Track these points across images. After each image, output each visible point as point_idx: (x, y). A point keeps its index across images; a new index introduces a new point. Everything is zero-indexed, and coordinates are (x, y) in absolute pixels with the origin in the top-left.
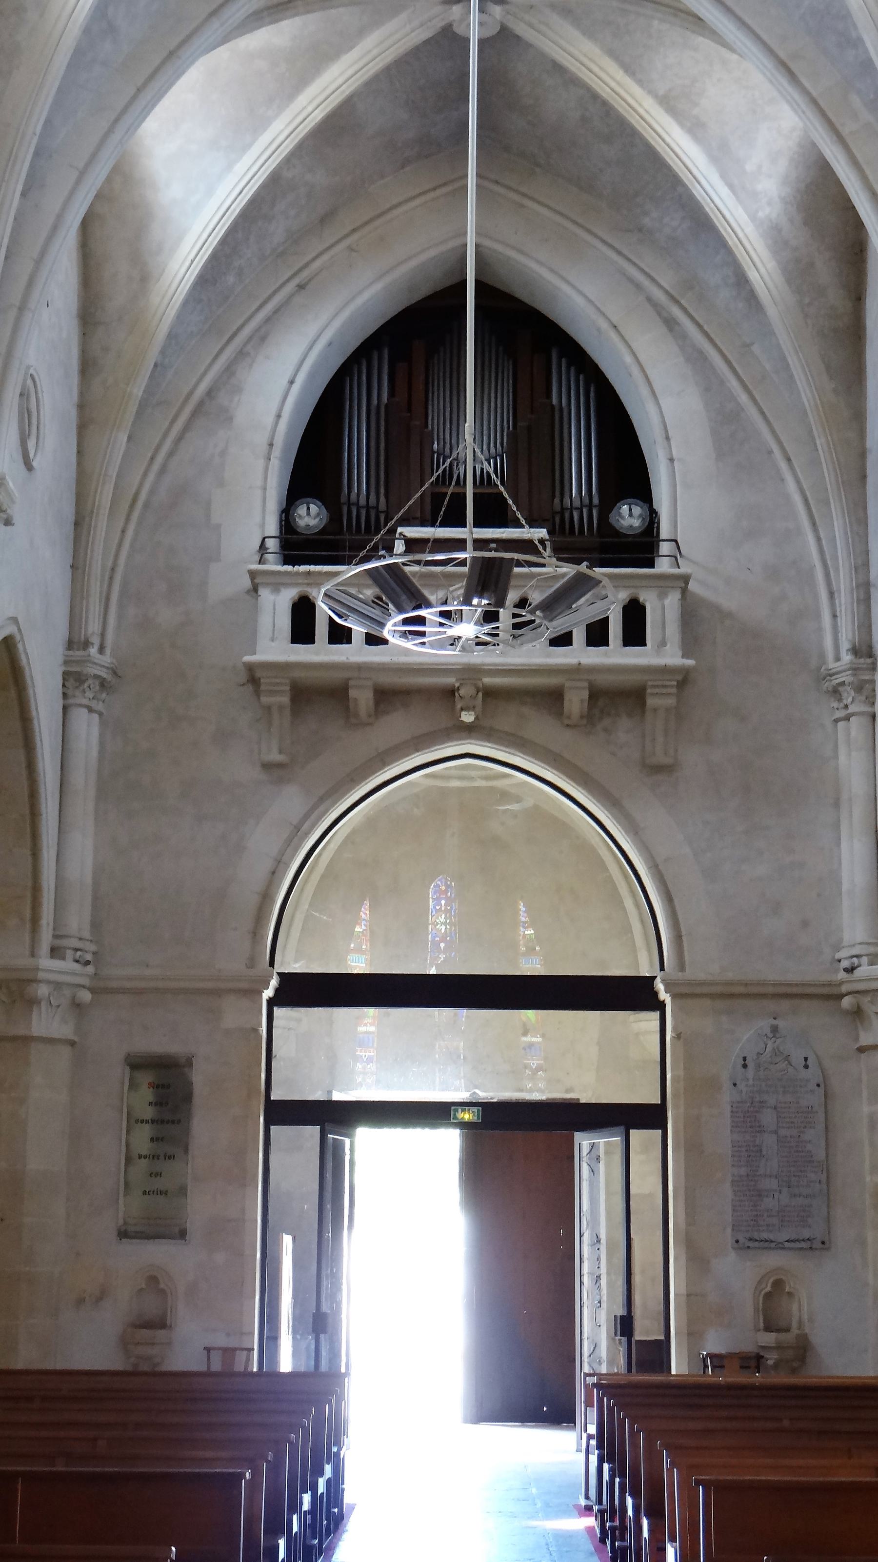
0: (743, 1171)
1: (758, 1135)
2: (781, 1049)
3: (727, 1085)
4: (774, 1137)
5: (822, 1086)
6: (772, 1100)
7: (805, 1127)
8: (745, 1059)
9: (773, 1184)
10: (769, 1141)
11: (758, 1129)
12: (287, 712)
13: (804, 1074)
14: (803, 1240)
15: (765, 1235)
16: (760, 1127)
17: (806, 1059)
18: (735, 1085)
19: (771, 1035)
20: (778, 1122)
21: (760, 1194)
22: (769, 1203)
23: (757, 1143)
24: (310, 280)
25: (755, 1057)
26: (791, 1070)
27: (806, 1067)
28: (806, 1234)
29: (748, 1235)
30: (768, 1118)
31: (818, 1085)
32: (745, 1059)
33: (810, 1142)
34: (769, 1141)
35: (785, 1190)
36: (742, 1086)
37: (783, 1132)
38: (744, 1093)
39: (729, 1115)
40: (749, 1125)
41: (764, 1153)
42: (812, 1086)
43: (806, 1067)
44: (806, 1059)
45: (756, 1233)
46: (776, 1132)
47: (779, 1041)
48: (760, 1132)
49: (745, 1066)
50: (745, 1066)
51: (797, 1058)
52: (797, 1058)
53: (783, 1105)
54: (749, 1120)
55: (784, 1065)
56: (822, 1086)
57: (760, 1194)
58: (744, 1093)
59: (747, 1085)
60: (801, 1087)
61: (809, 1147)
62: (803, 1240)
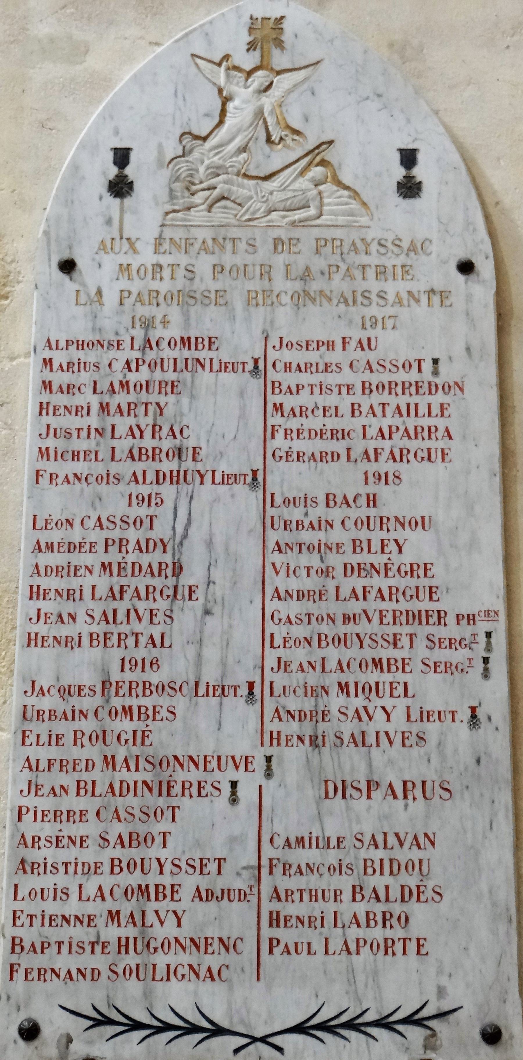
0: (84, 666)
1: (168, 491)
2: (303, 282)
3: (34, 270)
4: (247, 501)
5: (485, 268)
6: (242, 342)
7: (400, 456)
8: (122, 157)
9: (236, 729)
10: (221, 522)
11: (168, 466)
12: (244, 698)
13: (398, 217)
14: (383, 1023)
15: (178, 998)
16: (179, 453)
17: (409, 158)
18: (68, 266)
19: (248, 61)
20: (269, 433)
21: (166, 781)
22: (208, 826)
23: (162, 530)
24: (190, 514)
25: (172, 148)
26: (333, 197)
27: (410, 188)
28: (399, 986)
29: (86, 997)
30: (218, 416)
31: (466, 267)
32: (122, 157)
33: (422, 523)
34: (221, 522)
35: (292, 758)
36: (98, 272)
37: (288, 479)
38: (111, 298)
39: (27, 395)
40: (123, 445)
41: (193, 575)
42: (437, 270)
43: (410, 188)
44: (409, 158)
45: (133, 987)
46: (255, 480)
47: (283, 83)
48: (177, 478)
49: (120, 187)
50: (120, 187)
51: (368, 159)
52: (368, 159)
53: (287, 356)
54: (123, 424)
55: (304, 183)
56: (485, 268)
57: (166, 781)
58: (111, 298)
59: (125, 269)
60: (381, 272)
61: (418, 546)
62: (383, 1023)
